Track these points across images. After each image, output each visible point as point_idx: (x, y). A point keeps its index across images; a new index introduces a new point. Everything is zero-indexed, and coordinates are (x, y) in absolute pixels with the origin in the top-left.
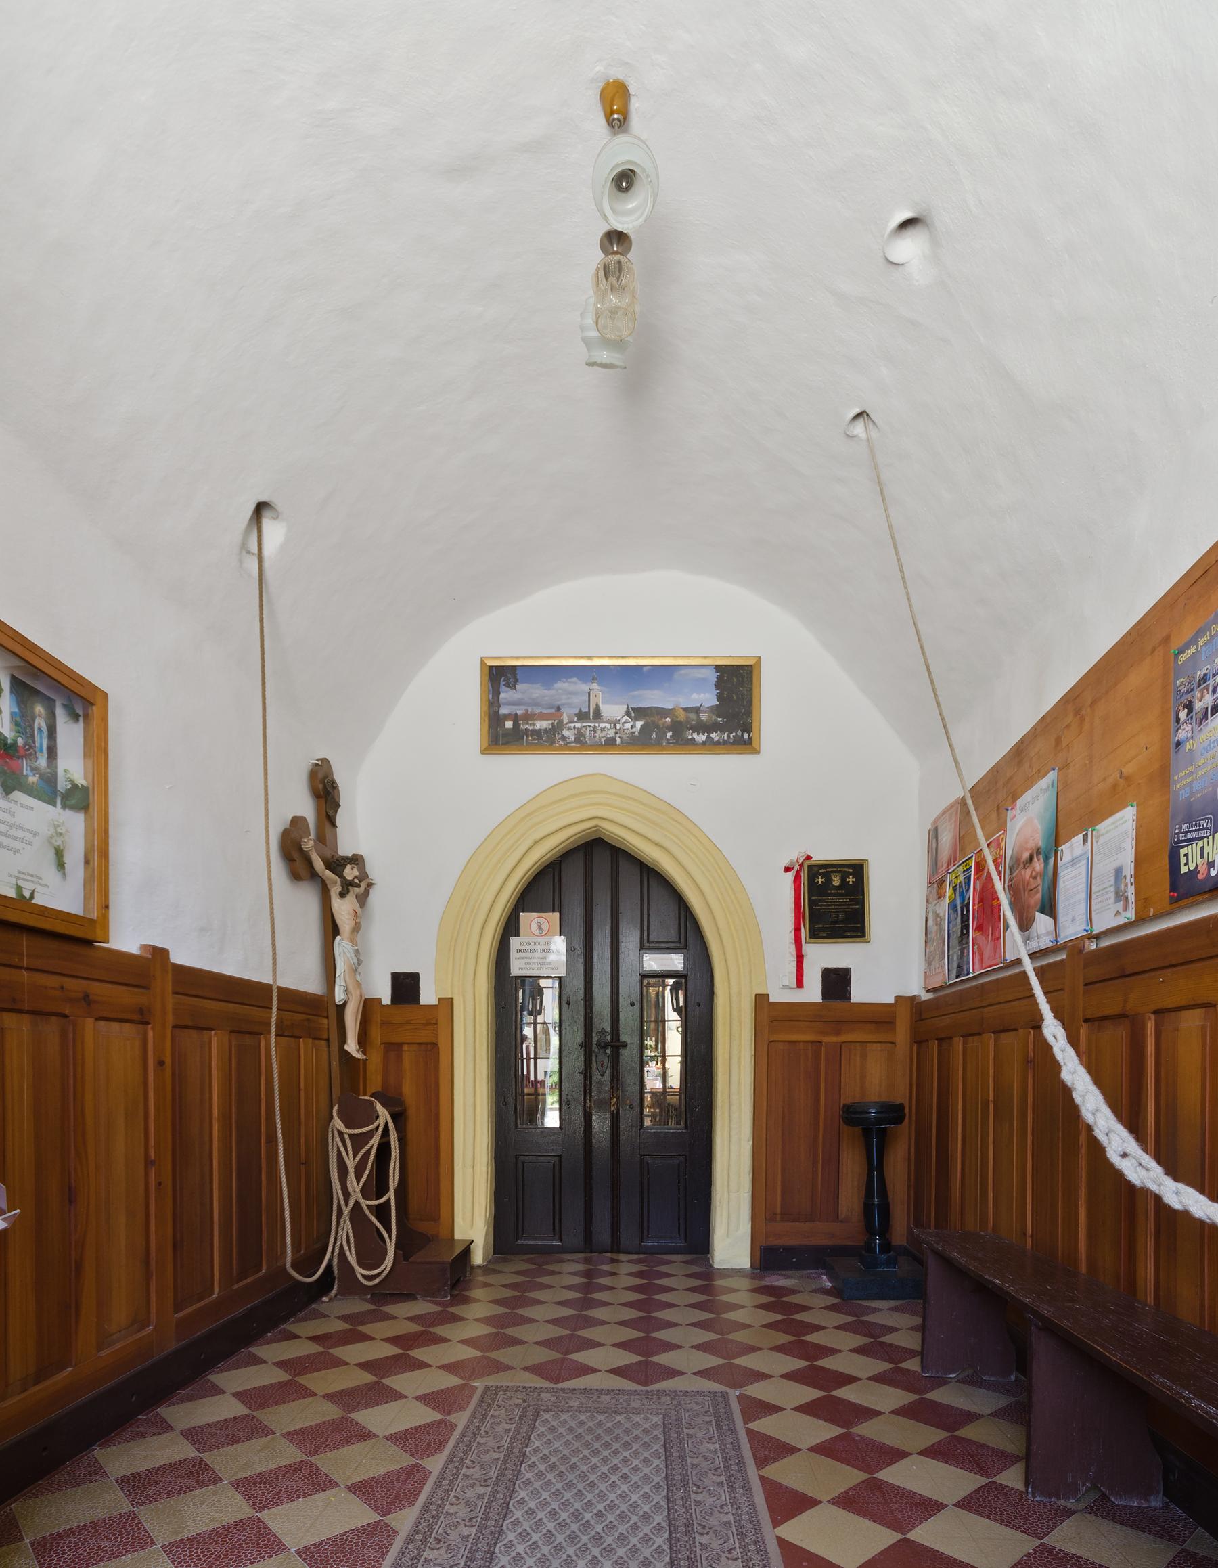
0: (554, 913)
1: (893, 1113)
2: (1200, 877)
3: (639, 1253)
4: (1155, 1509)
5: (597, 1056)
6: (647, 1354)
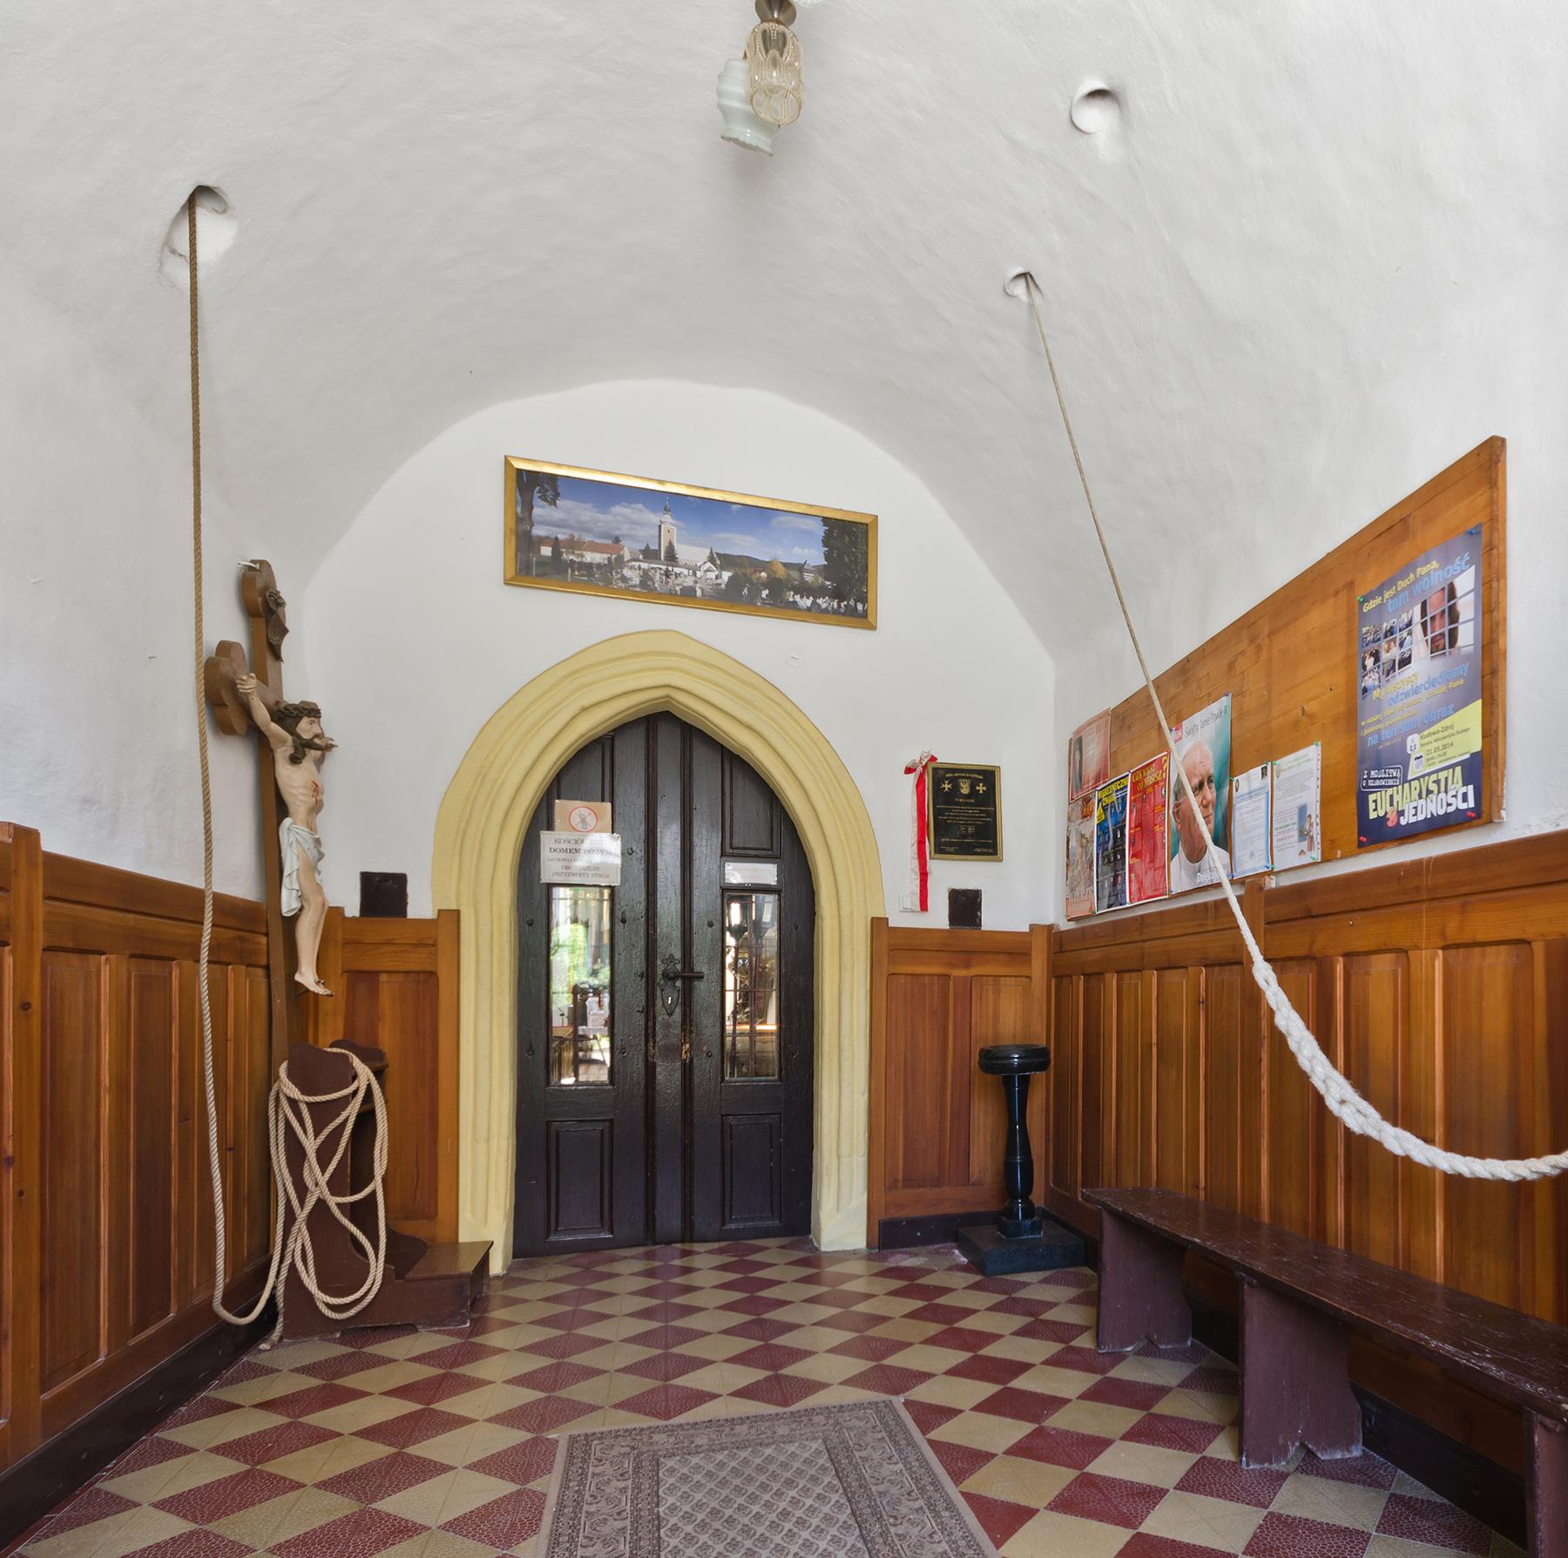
0: (604, 804)
1: (1037, 1058)
2: (1390, 824)
3: (719, 1240)
4: (1356, 1459)
5: (662, 990)
6: (774, 1367)
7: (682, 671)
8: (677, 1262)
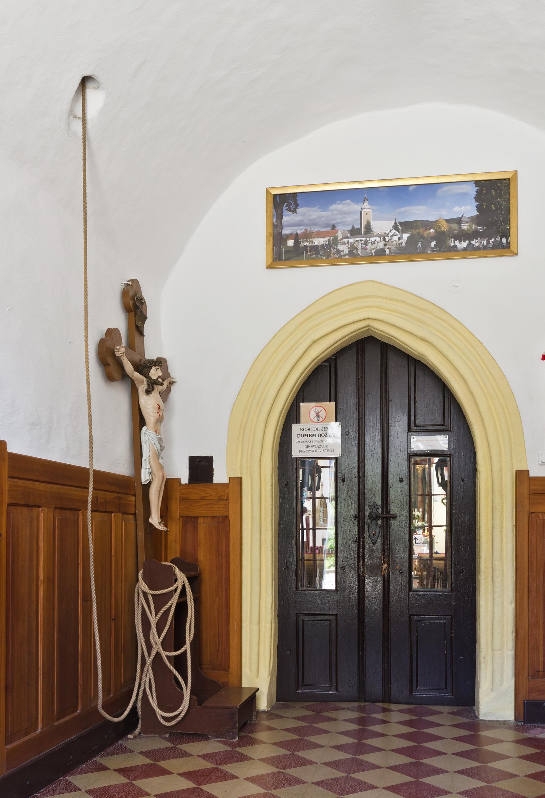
5: (369, 527)
7: (378, 307)
8: (379, 716)
